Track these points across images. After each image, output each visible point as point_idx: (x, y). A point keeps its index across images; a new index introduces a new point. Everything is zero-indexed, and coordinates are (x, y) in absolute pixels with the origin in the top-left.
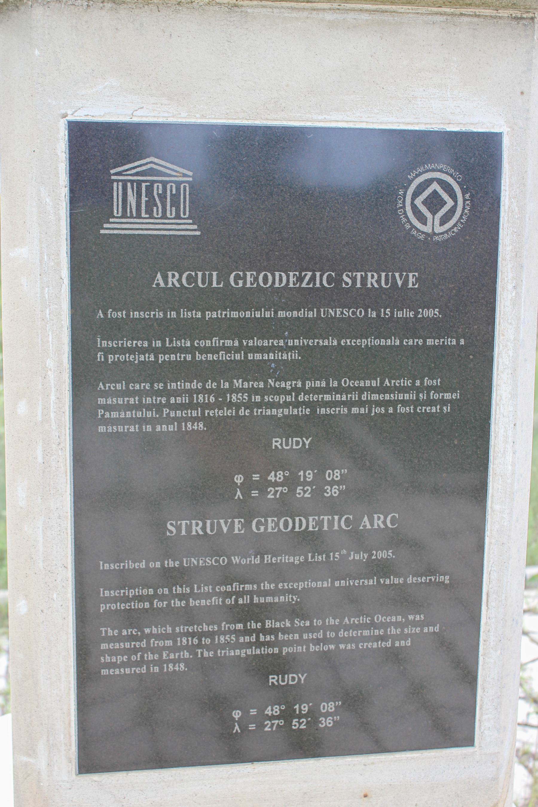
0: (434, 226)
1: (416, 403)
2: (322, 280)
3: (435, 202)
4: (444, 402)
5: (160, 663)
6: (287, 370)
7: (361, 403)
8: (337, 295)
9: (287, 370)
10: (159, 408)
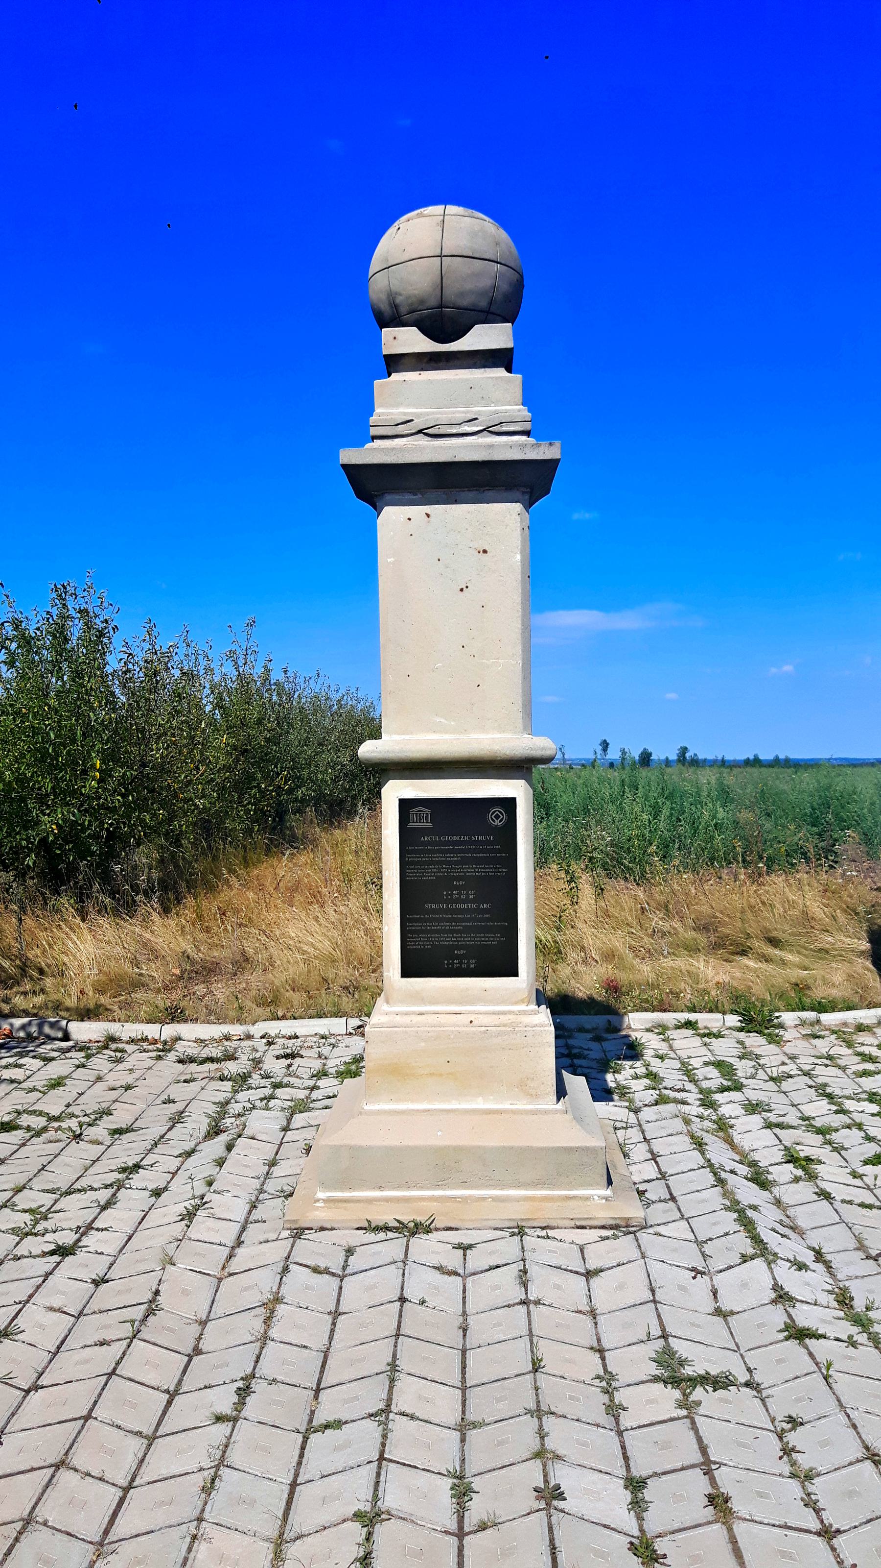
0: (497, 823)
1: (495, 872)
2: (466, 838)
3: (497, 817)
4: (502, 872)
5: (424, 945)
6: (456, 863)
7: (478, 872)
8: (470, 842)
9: (456, 863)
10: (423, 873)
